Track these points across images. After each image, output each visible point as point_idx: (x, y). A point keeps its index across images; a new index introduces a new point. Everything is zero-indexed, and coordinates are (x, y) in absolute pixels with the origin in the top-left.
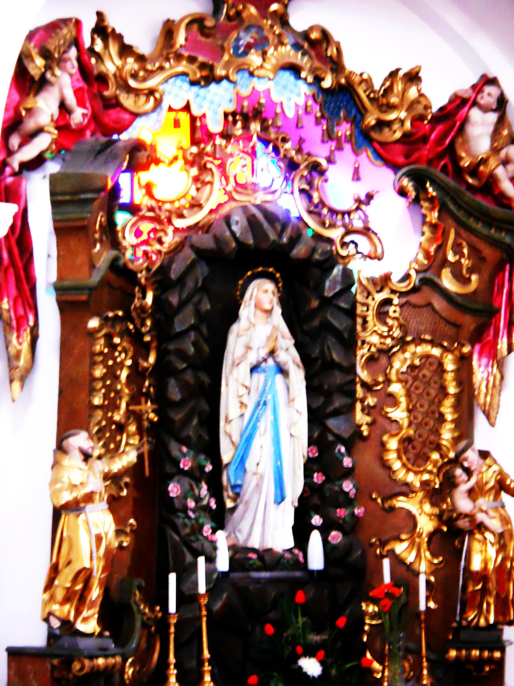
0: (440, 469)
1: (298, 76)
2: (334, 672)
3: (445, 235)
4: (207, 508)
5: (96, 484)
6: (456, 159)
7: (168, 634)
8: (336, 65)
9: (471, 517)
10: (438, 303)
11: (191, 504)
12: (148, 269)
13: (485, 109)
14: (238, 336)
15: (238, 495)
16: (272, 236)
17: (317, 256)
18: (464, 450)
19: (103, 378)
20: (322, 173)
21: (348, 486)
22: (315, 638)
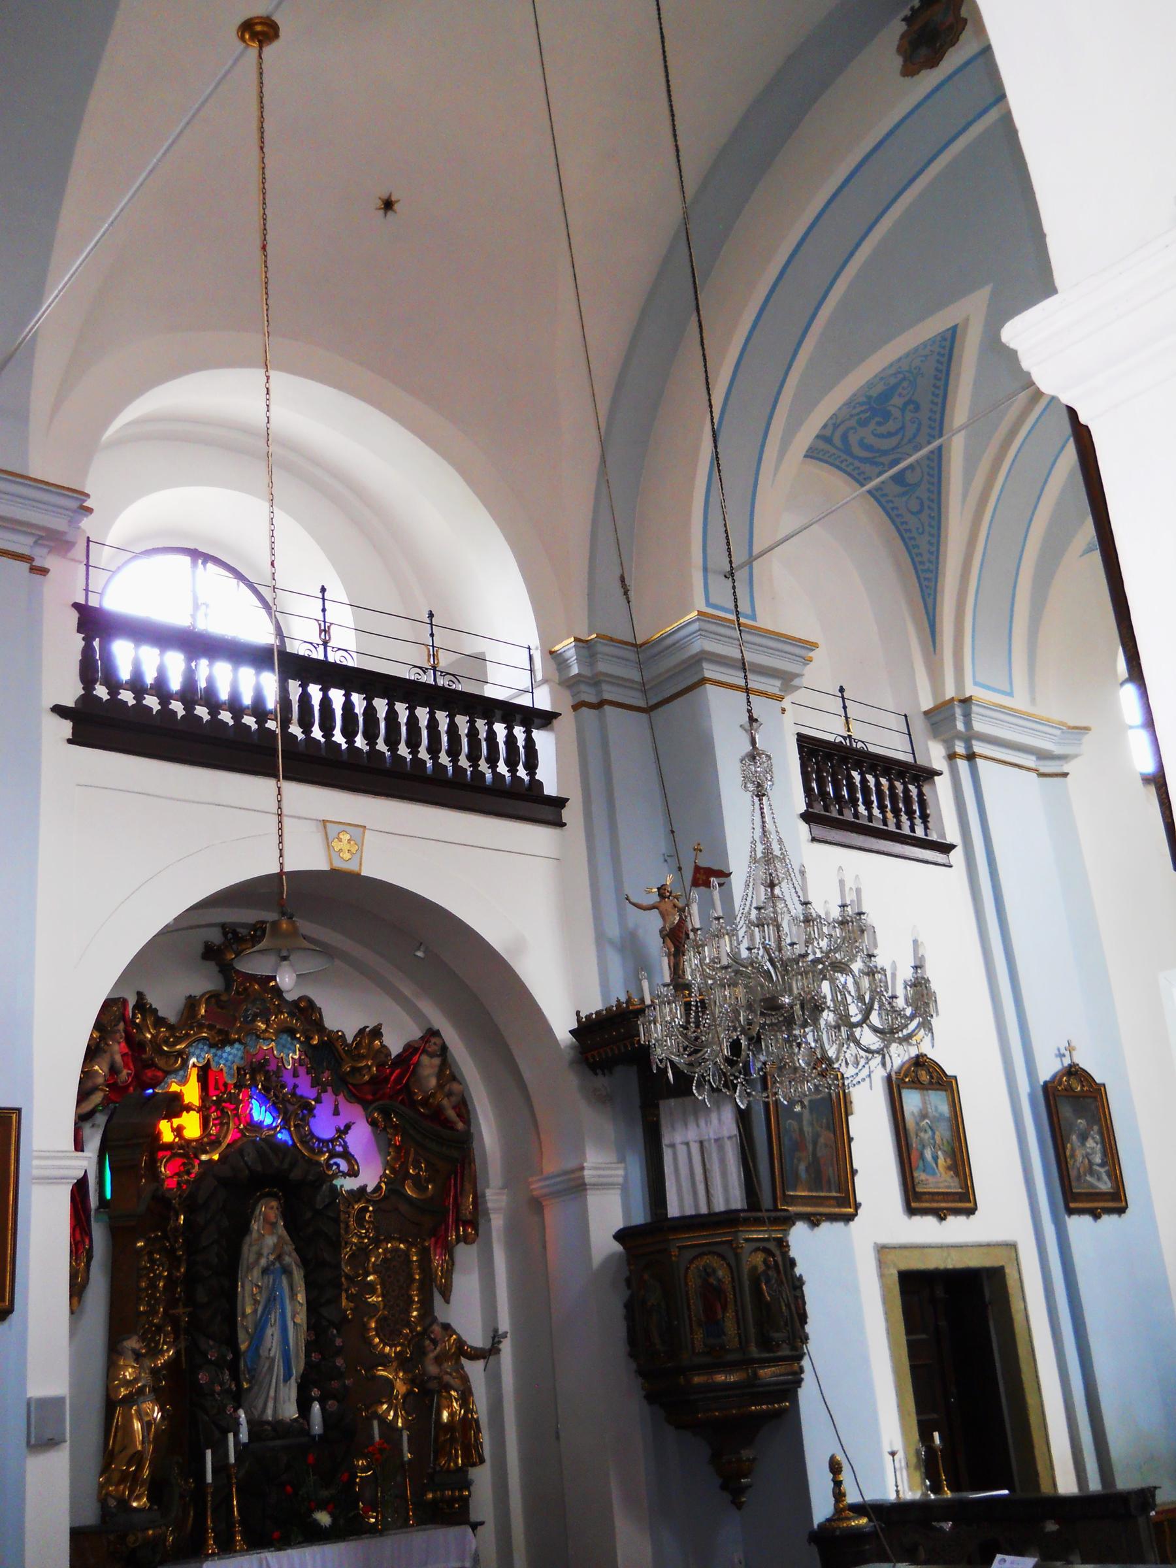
0: (409, 1342)
1: (294, 1038)
2: (342, 1522)
3: (407, 1153)
4: (229, 1391)
5: (145, 1380)
6: (411, 1094)
7: (205, 1503)
8: (319, 1026)
9: (438, 1378)
10: (404, 1208)
11: (218, 1388)
12: (180, 1196)
13: (432, 1055)
14: (251, 1245)
15: (253, 1377)
16: (276, 1164)
17: (310, 1177)
18: (431, 1325)
19: (146, 1289)
20: (311, 1110)
21: (339, 1362)
22: (325, 1493)
